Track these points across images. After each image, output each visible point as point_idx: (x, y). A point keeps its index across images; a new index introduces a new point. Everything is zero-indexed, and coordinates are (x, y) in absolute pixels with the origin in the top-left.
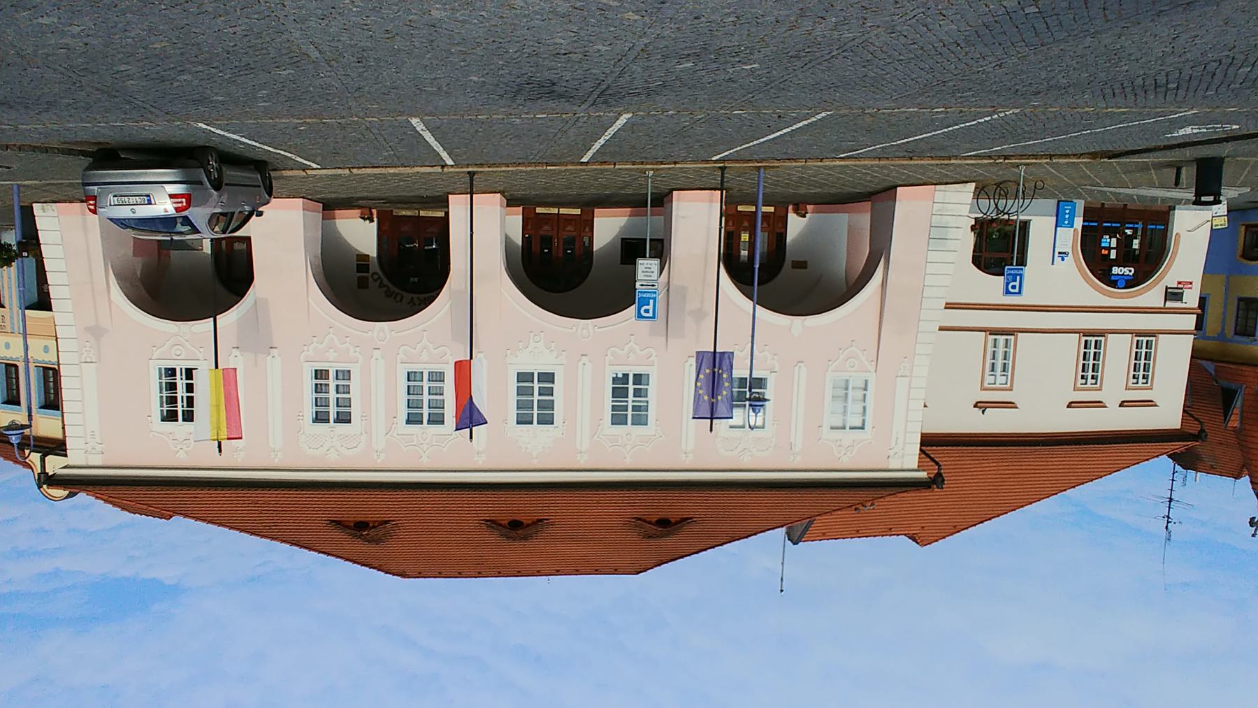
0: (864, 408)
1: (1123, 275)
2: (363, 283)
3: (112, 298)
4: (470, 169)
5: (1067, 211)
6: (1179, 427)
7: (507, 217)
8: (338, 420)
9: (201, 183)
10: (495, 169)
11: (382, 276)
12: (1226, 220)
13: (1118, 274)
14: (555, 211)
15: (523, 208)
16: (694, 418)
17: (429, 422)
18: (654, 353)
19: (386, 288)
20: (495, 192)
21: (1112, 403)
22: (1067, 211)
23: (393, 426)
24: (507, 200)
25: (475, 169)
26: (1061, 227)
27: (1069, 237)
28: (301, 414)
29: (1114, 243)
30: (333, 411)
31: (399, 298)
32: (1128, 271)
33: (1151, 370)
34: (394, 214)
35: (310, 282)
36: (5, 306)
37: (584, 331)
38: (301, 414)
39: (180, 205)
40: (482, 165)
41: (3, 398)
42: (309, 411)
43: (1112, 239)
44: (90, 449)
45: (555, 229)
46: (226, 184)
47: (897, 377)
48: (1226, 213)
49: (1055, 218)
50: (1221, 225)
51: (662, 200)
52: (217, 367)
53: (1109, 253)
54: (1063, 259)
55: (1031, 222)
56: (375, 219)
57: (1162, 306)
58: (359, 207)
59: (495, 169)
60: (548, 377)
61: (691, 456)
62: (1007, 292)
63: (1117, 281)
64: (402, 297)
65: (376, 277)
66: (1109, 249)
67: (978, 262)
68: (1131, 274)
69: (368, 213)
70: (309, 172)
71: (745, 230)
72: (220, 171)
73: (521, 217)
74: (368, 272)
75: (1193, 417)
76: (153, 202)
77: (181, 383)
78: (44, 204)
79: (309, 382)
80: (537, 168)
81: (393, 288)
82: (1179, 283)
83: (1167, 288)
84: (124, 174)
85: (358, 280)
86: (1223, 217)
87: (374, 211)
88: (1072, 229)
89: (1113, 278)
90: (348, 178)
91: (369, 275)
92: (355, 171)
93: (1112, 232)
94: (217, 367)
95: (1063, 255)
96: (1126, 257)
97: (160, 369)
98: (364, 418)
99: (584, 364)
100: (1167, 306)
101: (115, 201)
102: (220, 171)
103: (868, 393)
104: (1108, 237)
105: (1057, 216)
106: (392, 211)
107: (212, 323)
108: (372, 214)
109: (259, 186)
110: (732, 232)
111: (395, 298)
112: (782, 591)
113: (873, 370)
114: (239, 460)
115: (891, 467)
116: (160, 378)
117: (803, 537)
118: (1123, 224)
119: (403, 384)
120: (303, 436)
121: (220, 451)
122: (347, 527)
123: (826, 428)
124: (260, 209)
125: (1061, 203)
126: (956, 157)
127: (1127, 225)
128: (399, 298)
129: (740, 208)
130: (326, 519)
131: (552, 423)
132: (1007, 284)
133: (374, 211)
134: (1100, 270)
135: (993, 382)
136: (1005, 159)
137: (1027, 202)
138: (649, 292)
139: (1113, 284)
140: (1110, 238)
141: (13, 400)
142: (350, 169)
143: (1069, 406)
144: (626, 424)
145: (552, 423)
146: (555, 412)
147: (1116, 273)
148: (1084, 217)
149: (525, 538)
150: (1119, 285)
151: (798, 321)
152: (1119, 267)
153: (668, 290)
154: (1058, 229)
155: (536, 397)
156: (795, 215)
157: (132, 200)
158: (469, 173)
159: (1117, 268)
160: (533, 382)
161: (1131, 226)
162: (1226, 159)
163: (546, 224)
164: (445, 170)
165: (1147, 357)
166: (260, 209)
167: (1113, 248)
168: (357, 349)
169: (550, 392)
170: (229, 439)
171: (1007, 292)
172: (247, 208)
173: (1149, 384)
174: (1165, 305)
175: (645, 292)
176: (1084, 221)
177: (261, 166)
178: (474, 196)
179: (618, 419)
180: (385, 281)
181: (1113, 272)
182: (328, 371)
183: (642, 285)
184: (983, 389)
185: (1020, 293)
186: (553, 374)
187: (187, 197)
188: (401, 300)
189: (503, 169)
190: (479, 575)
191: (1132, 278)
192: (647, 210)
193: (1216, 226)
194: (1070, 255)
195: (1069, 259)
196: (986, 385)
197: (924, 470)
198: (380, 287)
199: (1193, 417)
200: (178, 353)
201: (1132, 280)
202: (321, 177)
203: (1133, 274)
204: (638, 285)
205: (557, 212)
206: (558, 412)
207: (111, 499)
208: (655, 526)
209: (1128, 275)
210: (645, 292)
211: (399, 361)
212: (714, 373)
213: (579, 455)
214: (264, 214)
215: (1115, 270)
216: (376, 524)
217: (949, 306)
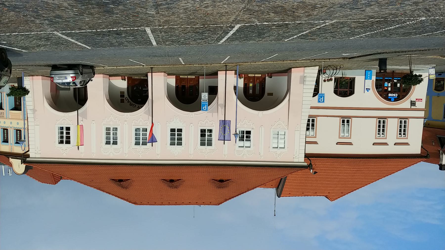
0: (285, 141)
1: (393, 96)
2: (122, 101)
3: (44, 105)
4: (151, 67)
5: (369, 74)
6: (420, 153)
7: (167, 79)
8: (113, 144)
9: (78, 73)
10: (158, 67)
11: (128, 99)
12: (435, 76)
13: (391, 96)
14: (186, 77)
15: (176, 76)
16: (218, 140)
17: (142, 144)
18: (214, 123)
19: (130, 103)
20: (162, 72)
21: (391, 144)
22: (369, 74)
23: (131, 146)
24: (168, 74)
25: (153, 67)
26: (367, 79)
27: (371, 83)
28: (102, 142)
29: (390, 85)
30: (112, 141)
31: (134, 105)
32: (395, 95)
33: (386, 127)
34: (133, 78)
35: (105, 99)
36: (4, 109)
37: (192, 116)
38: (102, 142)
39: (73, 79)
40: (154, 65)
41: (2, 140)
42: (104, 141)
43: (389, 83)
44: (36, 152)
45: (187, 83)
46: (84, 73)
47: (295, 131)
48: (435, 73)
49: (365, 76)
50: (433, 78)
51: (215, 74)
52: (78, 124)
53: (388, 89)
54: (368, 91)
55: (356, 78)
56: (126, 80)
57: (410, 108)
58: (121, 76)
59: (158, 67)
60: (180, 130)
61: (262, 157)
62: (319, 102)
63: (391, 99)
64: (135, 105)
65: (127, 99)
66: (388, 87)
67: (336, 92)
68: (396, 96)
69: (124, 78)
70: (105, 68)
71: (251, 82)
72: (82, 70)
73: (175, 79)
74: (124, 97)
75: (425, 149)
76: (67, 78)
77: (65, 131)
78: (26, 77)
79: (104, 132)
80: (171, 66)
81: (132, 103)
82: (417, 99)
83: (411, 101)
84: (57, 72)
85: (121, 100)
86: (434, 75)
87: (126, 77)
88: (371, 81)
89: (389, 98)
90: (116, 69)
91: (124, 98)
92: (118, 67)
93: (389, 81)
94: (78, 124)
95: (368, 89)
96: (395, 89)
97: (58, 127)
98: (121, 143)
99: (191, 126)
100: (412, 108)
101: (58, 78)
102: (82, 70)
103: (285, 136)
104: (387, 83)
105: (365, 76)
106: (132, 77)
107: (77, 112)
108: (125, 78)
109: (92, 73)
110: (246, 84)
111: (133, 106)
112: (275, 215)
113: (287, 128)
114: (82, 156)
115: (295, 161)
116: (58, 130)
117: (281, 195)
118: (393, 78)
119: (134, 132)
120: (102, 148)
121: (78, 149)
122: (116, 181)
123: (271, 148)
124: (92, 79)
125: (366, 71)
126: (298, 60)
127: (395, 78)
128: (134, 105)
129: (249, 75)
130: (109, 178)
131: (182, 145)
132: (319, 99)
133: (126, 77)
134: (384, 95)
135: (348, 136)
136: (314, 60)
137: (338, 71)
138: (205, 103)
139: (390, 100)
140: (388, 83)
141: (6, 141)
142: (116, 67)
143: (373, 145)
144: (205, 145)
145: (182, 145)
146: (182, 141)
147: (390, 96)
148: (376, 75)
149: (176, 187)
150: (392, 100)
151: (261, 112)
152: (391, 94)
153: (218, 103)
154: (366, 80)
155: (176, 137)
156: (268, 77)
157: (62, 78)
158: (151, 68)
159: (390, 94)
160: (175, 132)
161: (397, 78)
162: (388, 59)
163: (183, 81)
164: (144, 67)
165: (405, 126)
166: (92, 79)
167: (389, 87)
168: (120, 121)
169: (181, 135)
170: (81, 145)
171: (319, 102)
172: (89, 79)
173: (385, 137)
174: (411, 108)
175: (204, 103)
176: (376, 77)
177: (92, 67)
178: (153, 73)
179: (203, 144)
180: (130, 101)
181: (389, 96)
182: (110, 128)
183: (203, 100)
184: (340, 138)
185: (323, 102)
186: (182, 129)
187: (75, 77)
188: (135, 107)
189: (161, 66)
190: (162, 204)
191: (397, 97)
192: (204, 77)
193: (431, 78)
194: (371, 89)
195: (371, 91)
196: (341, 136)
197: (306, 163)
198: (128, 102)
199: (425, 149)
200: (64, 122)
201: (397, 98)
202: (108, 69)
203: (397, 96)
204: (202, 100)
205: (187, 77)
206: (183, 141)
207: (42, 169)
208: (218, 182)
209: (395, 97)
210: (204, 103)
211: (133, 125)
212: (225, 126)
213: (190, 155)
214: (93, 80)
215: (390, 95)
216: (125, 180)
217: (312, 108)
